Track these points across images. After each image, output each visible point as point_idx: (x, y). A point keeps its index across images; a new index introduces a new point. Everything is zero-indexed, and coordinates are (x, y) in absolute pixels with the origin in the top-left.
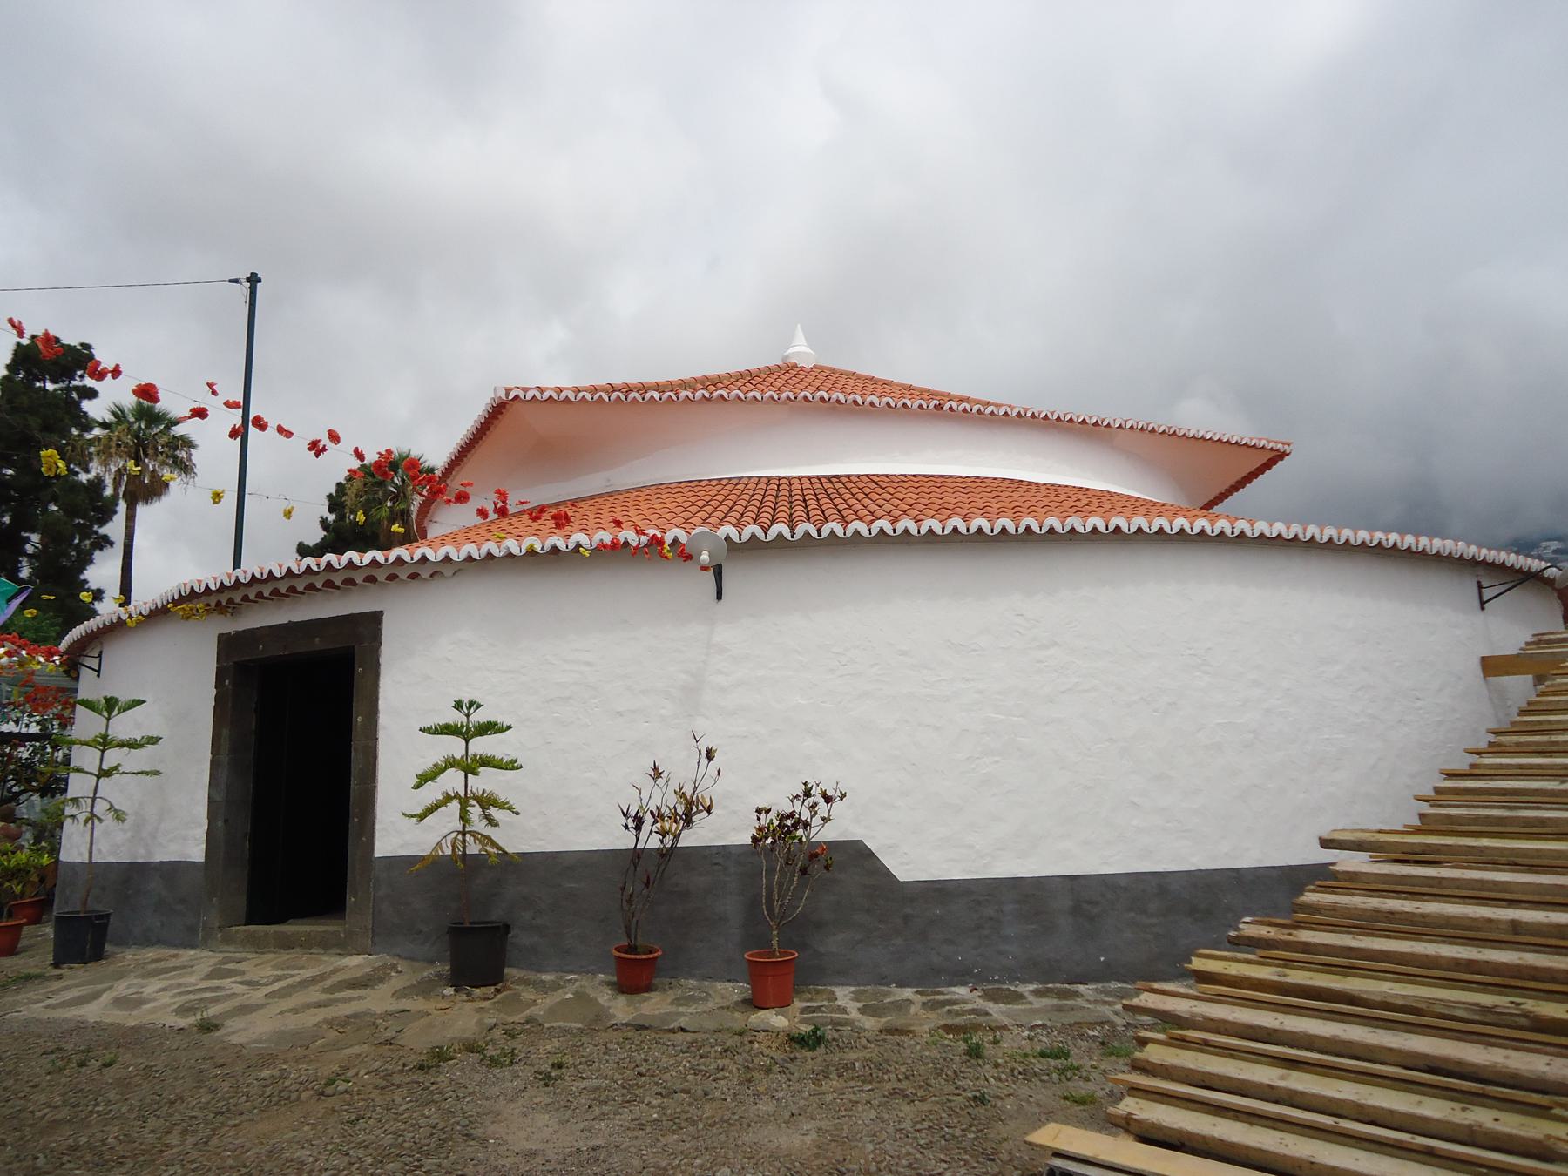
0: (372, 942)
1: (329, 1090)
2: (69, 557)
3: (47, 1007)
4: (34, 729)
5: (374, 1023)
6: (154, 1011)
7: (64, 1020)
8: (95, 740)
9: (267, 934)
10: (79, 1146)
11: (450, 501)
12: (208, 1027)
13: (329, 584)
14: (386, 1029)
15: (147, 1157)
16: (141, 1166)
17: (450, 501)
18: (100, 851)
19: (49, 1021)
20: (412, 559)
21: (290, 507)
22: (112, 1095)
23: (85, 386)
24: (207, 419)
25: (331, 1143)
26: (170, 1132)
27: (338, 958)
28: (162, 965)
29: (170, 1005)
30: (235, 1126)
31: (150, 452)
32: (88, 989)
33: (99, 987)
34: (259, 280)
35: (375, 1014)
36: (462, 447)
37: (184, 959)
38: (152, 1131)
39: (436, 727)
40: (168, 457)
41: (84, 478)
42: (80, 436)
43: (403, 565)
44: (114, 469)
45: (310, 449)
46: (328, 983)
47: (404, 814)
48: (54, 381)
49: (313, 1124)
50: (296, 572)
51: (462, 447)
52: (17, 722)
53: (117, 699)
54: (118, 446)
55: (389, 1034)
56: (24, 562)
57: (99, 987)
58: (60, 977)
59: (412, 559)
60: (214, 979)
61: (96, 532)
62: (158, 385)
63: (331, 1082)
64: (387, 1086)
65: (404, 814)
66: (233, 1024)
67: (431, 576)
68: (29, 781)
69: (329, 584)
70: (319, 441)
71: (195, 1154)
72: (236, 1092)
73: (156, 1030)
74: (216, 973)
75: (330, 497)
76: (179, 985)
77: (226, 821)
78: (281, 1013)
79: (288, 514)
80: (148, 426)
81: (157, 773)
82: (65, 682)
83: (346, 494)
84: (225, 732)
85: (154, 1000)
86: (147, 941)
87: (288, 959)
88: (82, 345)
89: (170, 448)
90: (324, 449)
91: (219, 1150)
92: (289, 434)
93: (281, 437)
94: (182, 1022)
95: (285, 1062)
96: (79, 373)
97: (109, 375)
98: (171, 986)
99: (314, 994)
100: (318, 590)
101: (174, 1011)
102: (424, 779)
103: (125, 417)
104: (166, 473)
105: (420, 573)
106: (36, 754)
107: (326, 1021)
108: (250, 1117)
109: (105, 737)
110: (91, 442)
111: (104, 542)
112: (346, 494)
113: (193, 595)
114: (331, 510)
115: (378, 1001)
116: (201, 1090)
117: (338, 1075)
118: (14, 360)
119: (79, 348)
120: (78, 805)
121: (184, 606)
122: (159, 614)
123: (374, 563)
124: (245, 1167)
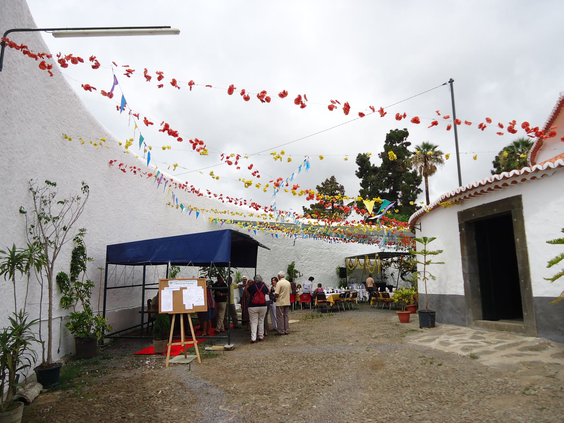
0: (537, 332)
1: (527, 392)
2: (410, 197)
3: (419, 341)
4: (407, 251)
5: (544, 367)
6: (454, 348)
7: (425, 346)
8: (422, 252)
9: (492, 324)
10: (432, 393)
11: (547, 137)
12: (474, 357)
13: (497, 187)
14: (550, 370)
15: (456, 403)
16: (454, 406)
17: (547, 137)
18: (429, 290)
19: (420, 346)
20: (531, 171)
21: (475, 155)
22: (442, 376)
23: (407, 142)
24: (438, 125)
25: (531, 417)
26: (463, 395)
27: (522, 337)
28: (455, 331)
29: (459, 346)
30: (488, 399)
31: (429, 159)
32: (431, 337)
33: (435, 337)
34: (453, 81)
35: (544, 363)
36: (548, 124)
37: (462, 330)
38: (457, 393)
39: (554, 241)
40: (435, 159)
41: (411, 171)
42: (408, 158)
43: (527, 174)
44: (419, 167)
45: (479, 128)
46: (520, 347)
47: (544, 279)
48: (398, 143)
49: (522, 406)
50: (483, 184)
51: (548, 124)
52: (402, 249)
53: (427, 238)
54: (419, 159)
55: (552, 373)
56: (398, 200)
57: (435, 337)
58: (422, 332)
59: (531, 171)
60: (474, 339)
61: (417, 188)
62: (419, 117)
63: (528, 389)
64: (555, 397)
65: (544, 279)
66: (483, 358)
67: (542, 176)
68: (408, 268)
69: (497, 187)
70: (482, 124)
71: (474, 407)
72: (487, 385)
73: (455, 355)
74: (473, 337)
75: (494, 162)
76: (461, 340)
77: (470, 281)
78: (502, 356)
79: (475, 158)
80: (428, 151)
81: (443, 263)
82: (411, 235)
83: (499, 160)
84: (465, 248)
85: (453, 344)
86: (449, 322)
87: (502, 335)
88: (404, 129)
89: (436, 156)
90: (485, 127)
91: (484, 407)
92: (470, 124)
93: (467, 125)
94: (464, 354)
95: (506, 376)
96: (405, 138)
97: (403, 117)
98: (458, 339)
99: (514, 350)
100: (493, 190)
101: (461, 349)
102: (552, 263)
103: (420, 149)
104: (435, 164)
105: (535, 177)
106: (409, 259)
107: (521, 363)
108: (494, 396)
109: (425, 251)
110: (411, 159)
111: (420, 191)
112: (499, 160)
113: (446, 199)
114: (495, 167)
115: (544, 357)
116: (474, 381)
117: (530, 387)
118: (387, 139)
119: (403, 130)
120: (420, 274)
121: (443, 203)
122: (437, 207)
123: (515, 175)
124: (495, 417)
